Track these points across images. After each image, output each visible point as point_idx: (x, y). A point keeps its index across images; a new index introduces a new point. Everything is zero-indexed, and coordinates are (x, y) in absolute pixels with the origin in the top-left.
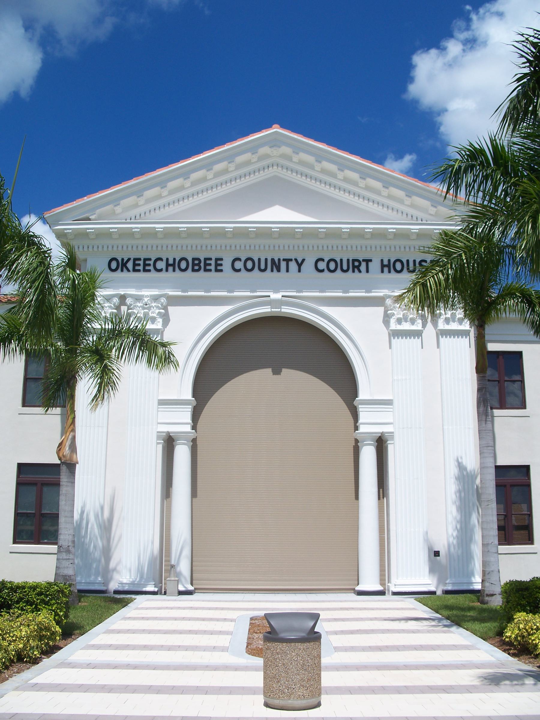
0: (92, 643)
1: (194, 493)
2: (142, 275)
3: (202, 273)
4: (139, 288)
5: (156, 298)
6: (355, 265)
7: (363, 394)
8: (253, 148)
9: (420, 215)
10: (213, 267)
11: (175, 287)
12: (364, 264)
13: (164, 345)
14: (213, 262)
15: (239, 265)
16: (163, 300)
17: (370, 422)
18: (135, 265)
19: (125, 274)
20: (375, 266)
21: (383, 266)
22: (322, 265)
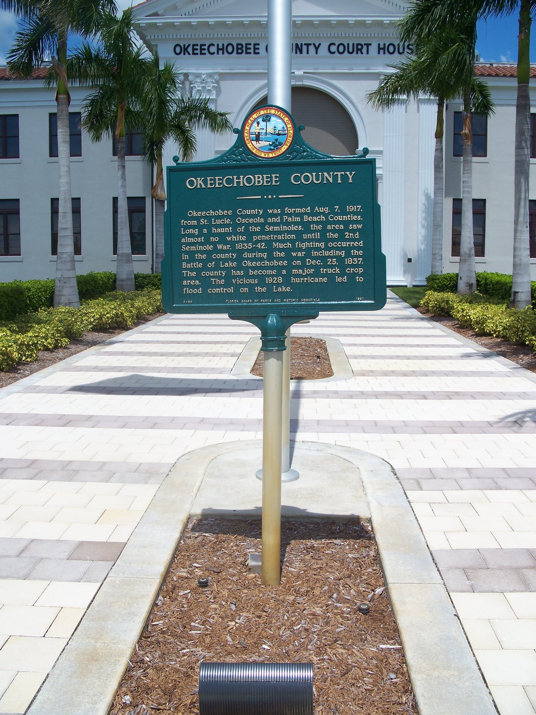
5: (210, 75)
6: (358, 49)
10: (252, 51)
13: (221, 115)
14: (252, 47)
16: (216, 77)
18: (194, 49)
20: (373, 49)
21: (379, 49)
22: (333, 49)
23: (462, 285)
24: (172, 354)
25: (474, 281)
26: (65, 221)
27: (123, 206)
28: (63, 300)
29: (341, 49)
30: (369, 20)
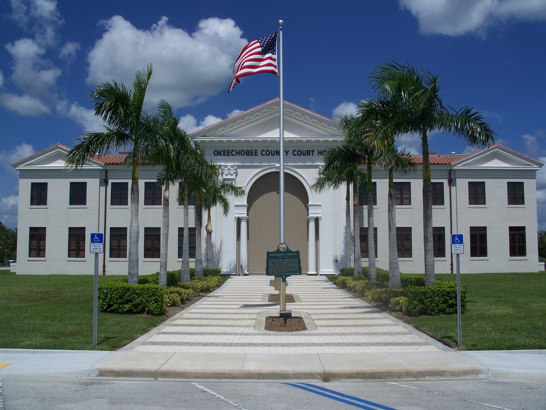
0: (149, 340)
1: (248, 239)
2: (227, 157)
3: (250, 156)
4: (226, 162)
5: (232, 166)
6: (308, 153)
7: (310, 203)
8: (269, 107)
9: (334, 133)
10: (254, 154)
11: (240, 162)
12: (311, 152)
13: (240, 188)
14: (254, 152)
15: (264, 153)
16: (235, 167)
17: (313, 213)
18: (224, 153)
19: (220, 157)
20: (316, 153)
21: (319, 153)
22: (295, 153)
23: (356, 273)
24: (195, 325)
25: (361, 271)
26: (186, 247)
27: (186, 233)
28: (185, 279)
29: (299, 153)
30: (313, 139)
